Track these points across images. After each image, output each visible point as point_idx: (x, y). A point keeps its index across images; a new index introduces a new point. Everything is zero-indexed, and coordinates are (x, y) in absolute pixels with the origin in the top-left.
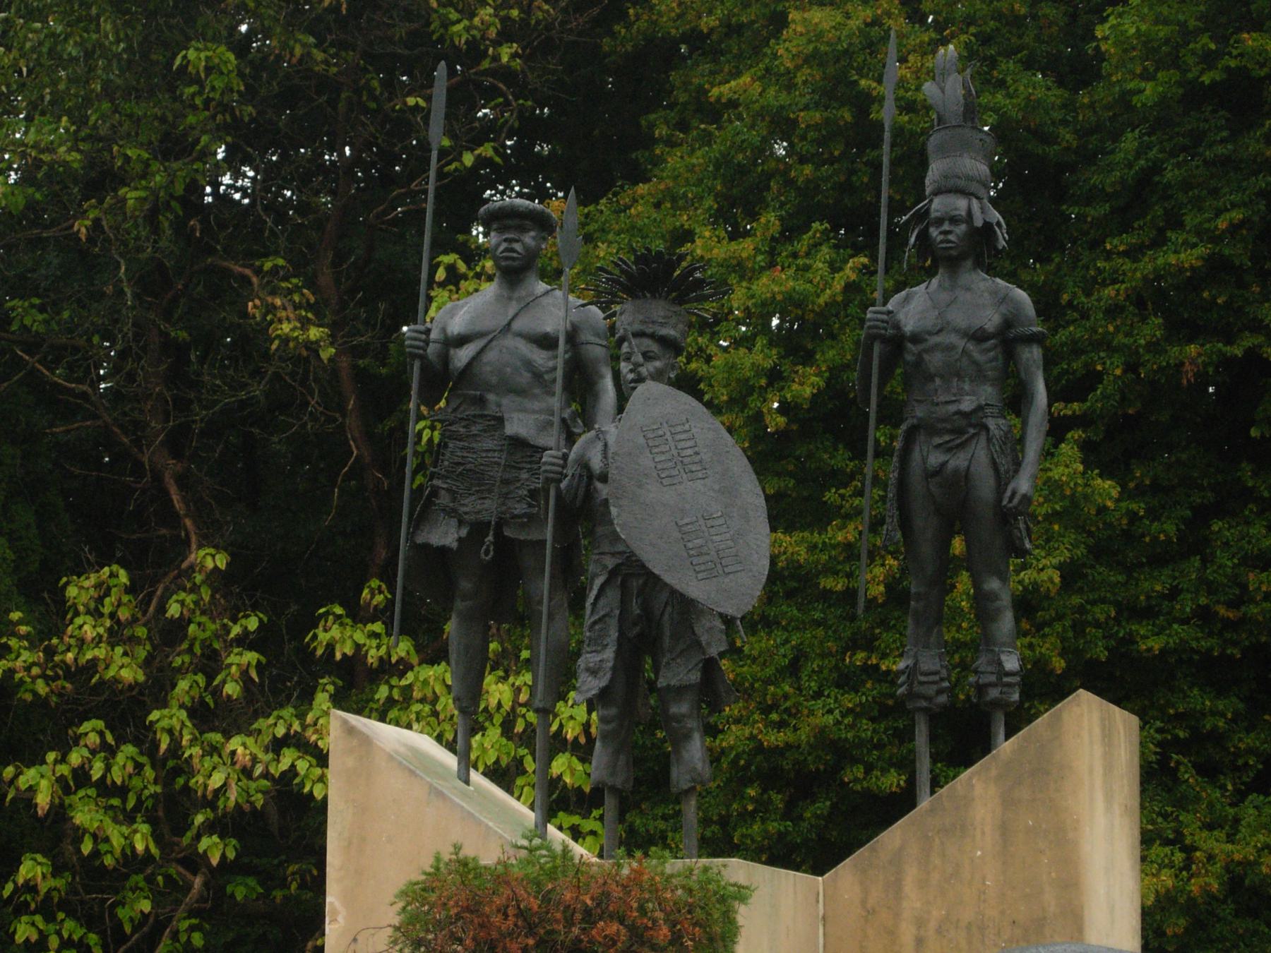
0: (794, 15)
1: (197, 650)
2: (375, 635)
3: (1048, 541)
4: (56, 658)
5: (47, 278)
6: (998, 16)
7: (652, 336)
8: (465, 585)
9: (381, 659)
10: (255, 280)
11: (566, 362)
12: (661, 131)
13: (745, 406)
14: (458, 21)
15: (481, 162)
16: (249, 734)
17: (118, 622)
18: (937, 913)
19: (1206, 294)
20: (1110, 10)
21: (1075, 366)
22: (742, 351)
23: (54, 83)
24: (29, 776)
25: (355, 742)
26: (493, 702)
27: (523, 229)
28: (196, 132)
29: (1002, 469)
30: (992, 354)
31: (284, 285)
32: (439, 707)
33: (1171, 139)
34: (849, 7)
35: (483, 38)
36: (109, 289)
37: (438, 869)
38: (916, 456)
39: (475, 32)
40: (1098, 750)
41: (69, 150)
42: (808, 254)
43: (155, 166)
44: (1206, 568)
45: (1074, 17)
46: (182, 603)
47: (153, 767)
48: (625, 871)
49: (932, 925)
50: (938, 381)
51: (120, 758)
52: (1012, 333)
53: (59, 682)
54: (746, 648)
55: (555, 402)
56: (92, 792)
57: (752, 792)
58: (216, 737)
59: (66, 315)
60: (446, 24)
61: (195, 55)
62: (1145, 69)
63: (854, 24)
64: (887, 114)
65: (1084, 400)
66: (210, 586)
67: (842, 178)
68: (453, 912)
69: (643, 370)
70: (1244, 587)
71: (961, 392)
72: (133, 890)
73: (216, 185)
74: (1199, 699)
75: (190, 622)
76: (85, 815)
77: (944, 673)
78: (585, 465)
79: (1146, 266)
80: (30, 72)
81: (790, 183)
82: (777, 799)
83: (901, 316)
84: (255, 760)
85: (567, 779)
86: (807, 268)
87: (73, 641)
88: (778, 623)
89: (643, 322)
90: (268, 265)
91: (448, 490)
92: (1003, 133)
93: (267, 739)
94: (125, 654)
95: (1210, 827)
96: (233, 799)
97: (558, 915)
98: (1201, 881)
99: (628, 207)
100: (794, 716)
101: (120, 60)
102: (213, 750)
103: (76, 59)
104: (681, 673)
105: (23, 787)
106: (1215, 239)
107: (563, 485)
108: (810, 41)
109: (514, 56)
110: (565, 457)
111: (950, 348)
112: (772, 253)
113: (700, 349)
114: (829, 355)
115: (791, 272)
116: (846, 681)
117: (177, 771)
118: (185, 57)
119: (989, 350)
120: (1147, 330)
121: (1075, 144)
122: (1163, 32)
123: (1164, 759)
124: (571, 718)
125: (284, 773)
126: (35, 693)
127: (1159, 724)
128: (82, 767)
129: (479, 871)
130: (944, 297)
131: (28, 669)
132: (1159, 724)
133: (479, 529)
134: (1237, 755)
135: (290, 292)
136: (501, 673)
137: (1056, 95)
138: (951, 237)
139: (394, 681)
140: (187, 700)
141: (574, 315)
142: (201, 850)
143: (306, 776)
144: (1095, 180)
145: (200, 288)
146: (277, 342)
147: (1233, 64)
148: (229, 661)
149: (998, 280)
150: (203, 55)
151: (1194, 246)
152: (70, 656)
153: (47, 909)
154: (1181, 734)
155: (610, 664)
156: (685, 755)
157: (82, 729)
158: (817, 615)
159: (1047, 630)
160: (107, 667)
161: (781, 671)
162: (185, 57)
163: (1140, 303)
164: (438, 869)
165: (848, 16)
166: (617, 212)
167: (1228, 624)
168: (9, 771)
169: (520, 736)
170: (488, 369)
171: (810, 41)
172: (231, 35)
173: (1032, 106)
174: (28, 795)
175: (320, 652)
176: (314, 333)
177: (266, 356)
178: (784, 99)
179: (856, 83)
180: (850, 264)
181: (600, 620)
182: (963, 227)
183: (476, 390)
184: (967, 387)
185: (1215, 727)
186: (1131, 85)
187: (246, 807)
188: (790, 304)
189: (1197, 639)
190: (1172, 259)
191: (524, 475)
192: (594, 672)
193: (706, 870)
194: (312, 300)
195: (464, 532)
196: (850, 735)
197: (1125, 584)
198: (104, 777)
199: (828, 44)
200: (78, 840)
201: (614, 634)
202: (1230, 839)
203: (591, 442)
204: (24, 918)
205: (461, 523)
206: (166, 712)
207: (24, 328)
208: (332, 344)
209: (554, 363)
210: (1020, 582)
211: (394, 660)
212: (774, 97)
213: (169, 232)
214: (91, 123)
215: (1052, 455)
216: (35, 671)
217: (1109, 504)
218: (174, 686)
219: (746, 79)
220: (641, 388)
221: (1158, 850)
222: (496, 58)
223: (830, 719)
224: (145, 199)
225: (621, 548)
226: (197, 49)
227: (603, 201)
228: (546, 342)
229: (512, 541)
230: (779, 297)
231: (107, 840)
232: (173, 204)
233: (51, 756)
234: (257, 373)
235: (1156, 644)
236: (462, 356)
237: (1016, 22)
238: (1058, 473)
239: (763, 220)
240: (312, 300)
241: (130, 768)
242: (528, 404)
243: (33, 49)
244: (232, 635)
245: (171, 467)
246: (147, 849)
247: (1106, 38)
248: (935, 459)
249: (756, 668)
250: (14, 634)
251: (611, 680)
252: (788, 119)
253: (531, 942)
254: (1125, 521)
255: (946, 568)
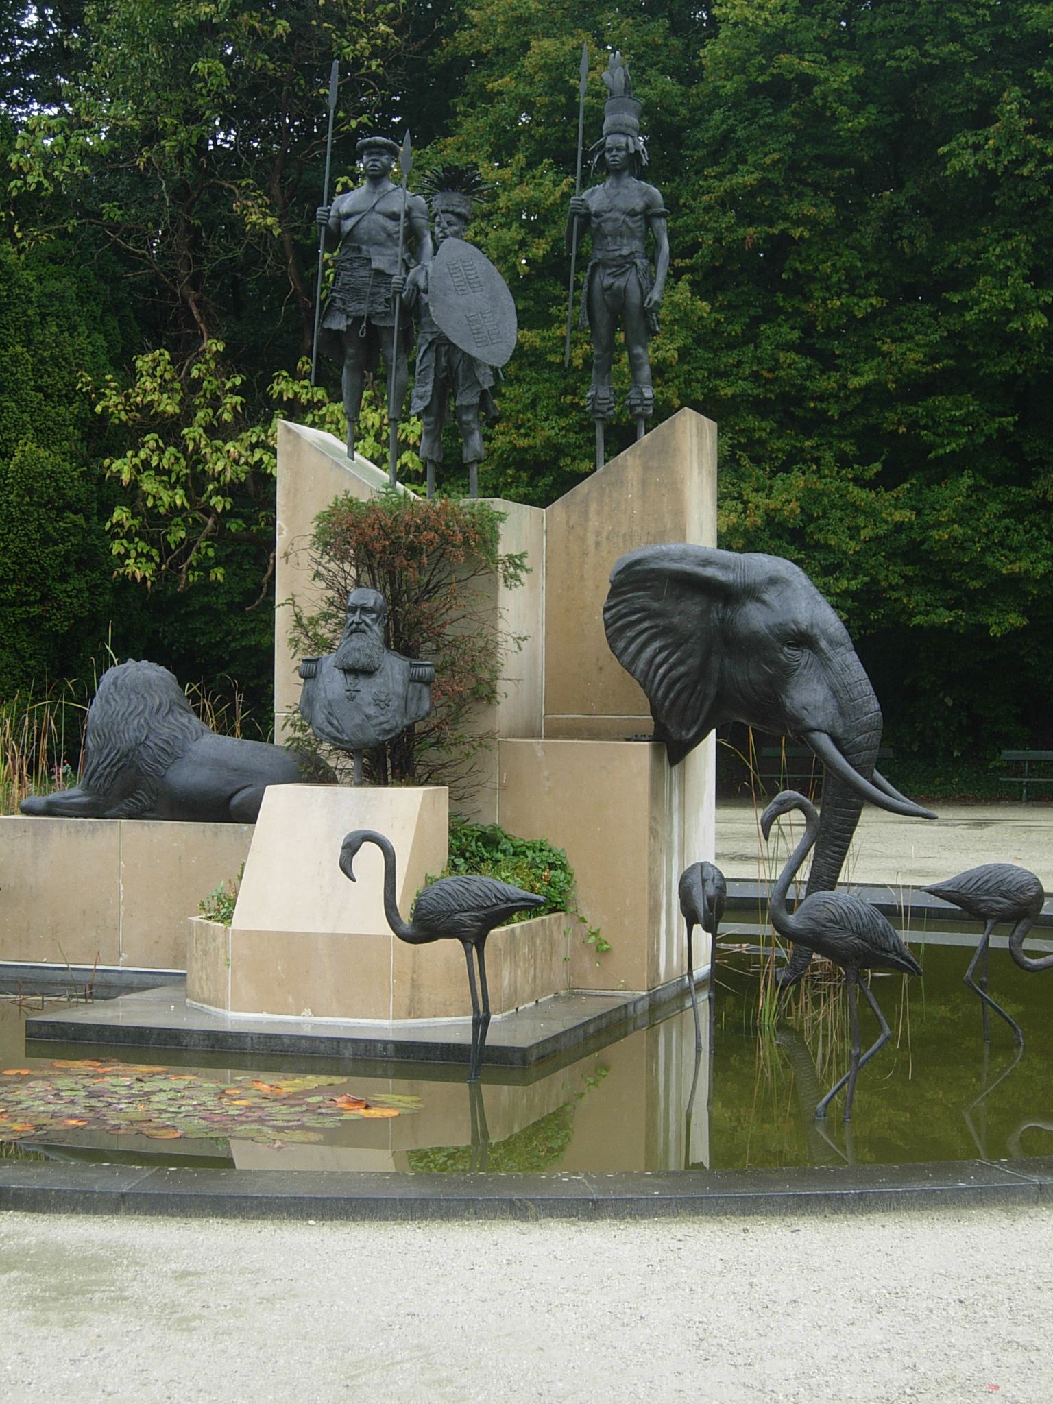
0: (533, 43)
1: (208, 395)
2: (306, 387)
3: (671, 335)
4: (132, 400)
5: (122, 191)
6: (646, 44)
7: (452, 212)
8: (351, 351)
9: (308, 400)
10: (237, 191)
11: (405, 228)
12: (460, 108)
13: (507, 260)
14: (348, 47)
15: (361, 125)
16: (237, 441)
17: (165, 380)
18: (607, 528)
19: (758, 200)
20: (708, 41)
21: (687, 239)
22: (505, 230)
23: (124, 82)
24: (118, 464)
25: (291, 437)
26: (370, 423)
27: (381, 154)
28: (203, 109)
29: (644, 287)
30: (639, 223)
31: (253, 194)
32: (340, 426)
33: (740, 114)
34: (564, 39)
35: (362, 56)
36: (156, 197)
37: (336, 504)
38: (597, 279)
39: (356, 53)
40: (695, 440)
41: (133, 119)
42: (541, 177)
43: (181, 128)
44: (756, 350)
45: (688, 46)
46: (199, 370)
47: (185, 459)
48: (438, 505)
49: (605, 534)
50: (609, 238)
51: (167, 454)
52: (650, 212)
53: (134, 413)
54: (507, 394)
55: (400, 250)
56: (152, 473)
57: (510, 472)
58: (219, 443)
59: (133, 211)
60: (341, 48)
61: (202, 66)
62: (727, 74)
63: (567, 48)
64: (583, 100)
65: (691, 258)
66: (215, 360)
67: (560, 134)
68: (344, 527)
69: (447, 231)
70: (777, 361)
71: (622, 245)
72: (175, 526)
73: (215, 140)
74: (752, 422)
75: (204, 380)
76: (148, 485)
77: (612, 399)
78: (416, 285)
79: (727, 184)
80: (111, 76)
81: (532, 137)
82: (524, 475)
83: (590, 203)
84: (240, 455)
85: (410, 465)
86: (540, 184)
87: (140, 391)
88: (525, 380)
89: (447, 205)
90: (244, 183)
91: (341, 299)
92: (647, 110)
93: (247, 444)
94: (169, 398)
95: (757, 491)
96: (228, 476)
97: (402, 528)
98: (752, 519)
99: (442, 150)
100: (533, 431)
101: (160, 68)
102: (218, 450)
103: (136, 68)
104: (468, 398)
105: (115, 470)
106: (764, 169)
107: (403, 295)
108: (542, 58)
109: (379, 66)
110: (405, 279)
111: (616, 220)
112: (521, 176)
113: (482, 229)
114: (553, 232)
115: (532, 186)
116: (561, 412)
117: (198, 462)
118: (196, 67)
119: (637, 221)
120: (726, 220)
121: (688, 116)
122: (737, 53)
123: (733, 454)
124: (412, 432)
125: (256, 462)
126: (120, 420)
127: (730, 435)
128: (146, 459)
129: (359, 505)
130: (613, 191)
131: (116, 406)
132: (730, 435)
133: (358, 320)
134: (772, 451)
135: (256, 198)
136: (374, 407)
137: (677, 89)
138: (617, 158)
139: (316, 412)
140: (203, 423)
141: (410, 202)
142: (212, 504)
143: (268, 464)
144: (699, 136)
145: (207, 196)
146: (249, 226)
147: (775, 71)
148: (225, 401)
149: (643, 183)
150: (206, 66)
151: (753, 173)
152: (139, 399)
153: (129, 536)
154: (743, 440)
155: (430, 393)
156: (471, 442)
157: (146, 439)
158: (546, 376)
159: (670, 384)
160: (159, 405)
161: (525, 406)
162: (196, 67)
163: (723, 204)
164: (336, 504)
165: (563, 44)
166: (436, 153)
167: (768, 381)
168: (107, 462)
169: (384, 442)
170: (362, 231)
171: (542, 58)
172: (221, 54)
173: (664, 94)
174: (118, 475)
175: (275, 396)
176: (270, 221)
177: (244, 234)
178: (528, 90)
179: (567, 81)
180: (564, 182)
181: (424, 370)
182: (624, 153)
183: (355, 242)
184: (625, 241)
185: (760, 437)
186: (719, 83)
187: (236, 481)
188: (532, 205)
189: (752, 389)
190: (740, 180)
191: (383, 290)
192: (421, 398)
193: (482, 504)
194: (269, 202)
195: (350, 322)
196: (563, 441)
197: (713, 359)
198: (158, 465)
199: (552, 59)
200: (145, 500)
201: (432, 377)
202: (768, 497)
203: (419, 271)
204: (117, 541)
205: (348, 317)
206: (191, 429)
207: (109, 218)
208: (280, 227)
209: (399, 228)
210: (656, 358)
211: (315, 400)
212: (523, 89)
213: (189, 165)
214: (145, 104)
215: (674, 288)
216: (120, 407)
217: (705, 315)
218: (196, 415)
219: (507, 79)
220: (446, 241)
221: (728, 503)
222: (369, 67)
223: (552, 432)
224: (175, 146)
225: (435, 330)
226: (203, 62)
227: (429, 147)
228: (394, 217)
229: (376, 327)
230: (525, 201)
231: (161, 499)
232: (191, 149)
233: (129, 453)
234: (239, 243)
235: (729, 392)
236: (348, 225)
237: (656, 48)
238: (677, 298)
239: (516, 158)
240: (269, 202)
241: (172, 460)
242: (384, 251)
243: (112, 63)
244: (227, 387)
245: (192, 295)
246: (183, 503)
247: (705, 57)
248: (607, 281)
249: (512, 405)
250: (108, 387)
251: (431, 402)
252: (530, 101)
253: (387, 543)
254: (713, 324)
255: (612, 346)
